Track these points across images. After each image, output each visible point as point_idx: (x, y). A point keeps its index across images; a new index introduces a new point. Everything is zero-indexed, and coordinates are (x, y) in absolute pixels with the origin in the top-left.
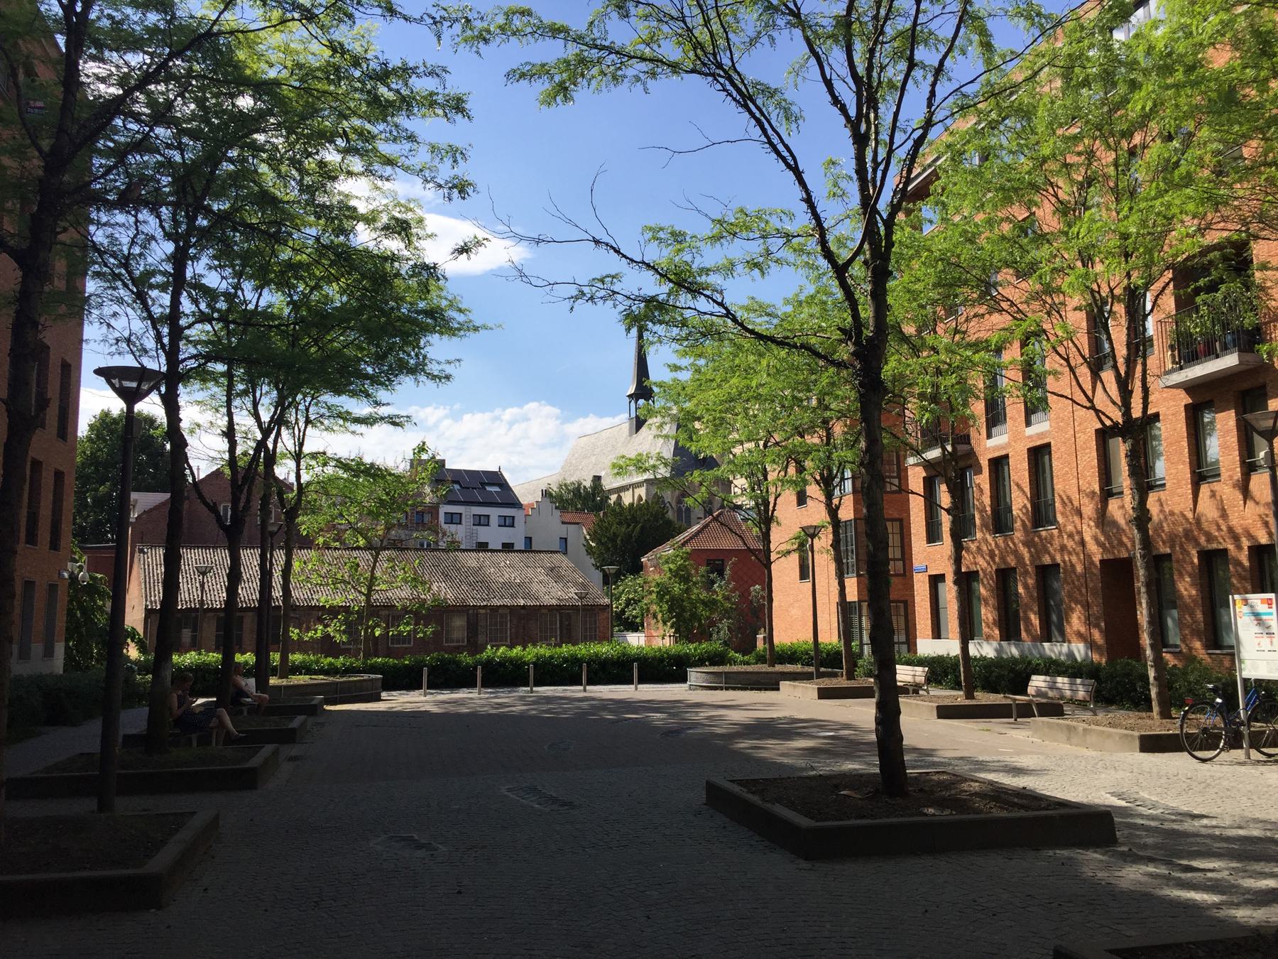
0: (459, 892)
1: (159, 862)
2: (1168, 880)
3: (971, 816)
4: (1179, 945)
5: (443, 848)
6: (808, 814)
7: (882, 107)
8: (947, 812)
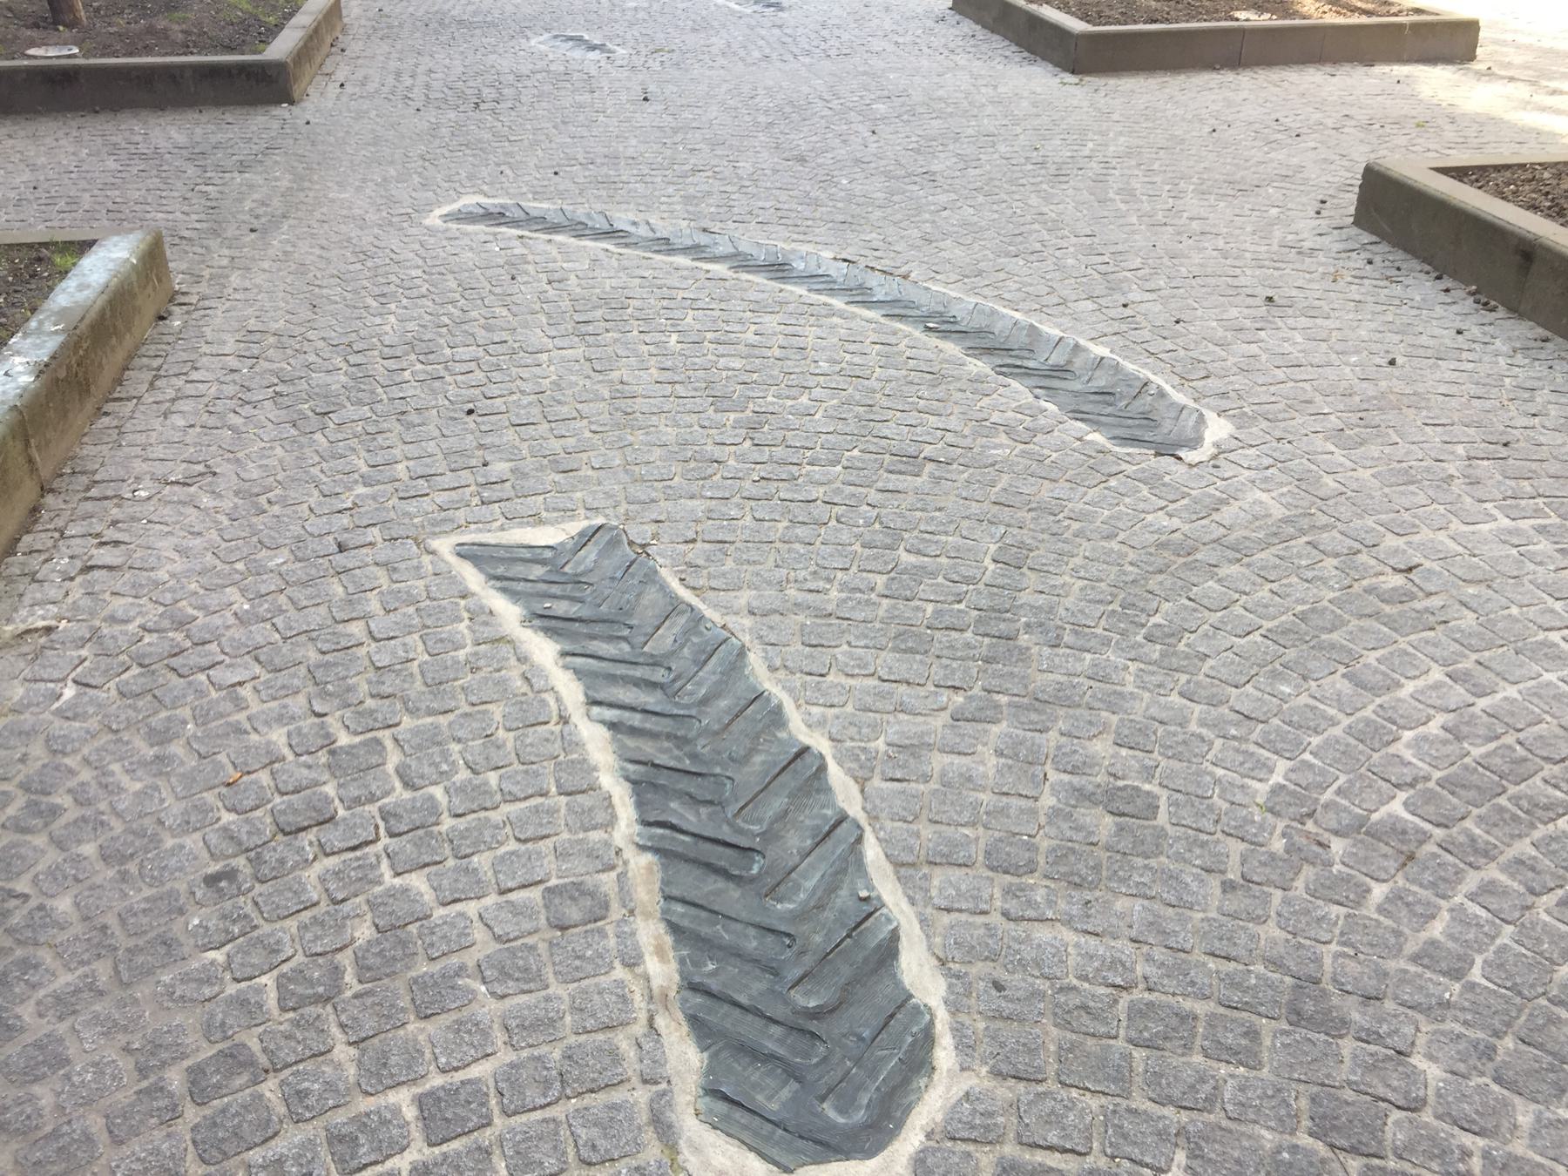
0: (646, 99)
1: (280, 48)
2: (1525, 105)
3: (1297, 22)
4: (1522, 166)
5: (621, 51)
6: (1085, 17)
7: (603, 732)
8: (1266, 16)
